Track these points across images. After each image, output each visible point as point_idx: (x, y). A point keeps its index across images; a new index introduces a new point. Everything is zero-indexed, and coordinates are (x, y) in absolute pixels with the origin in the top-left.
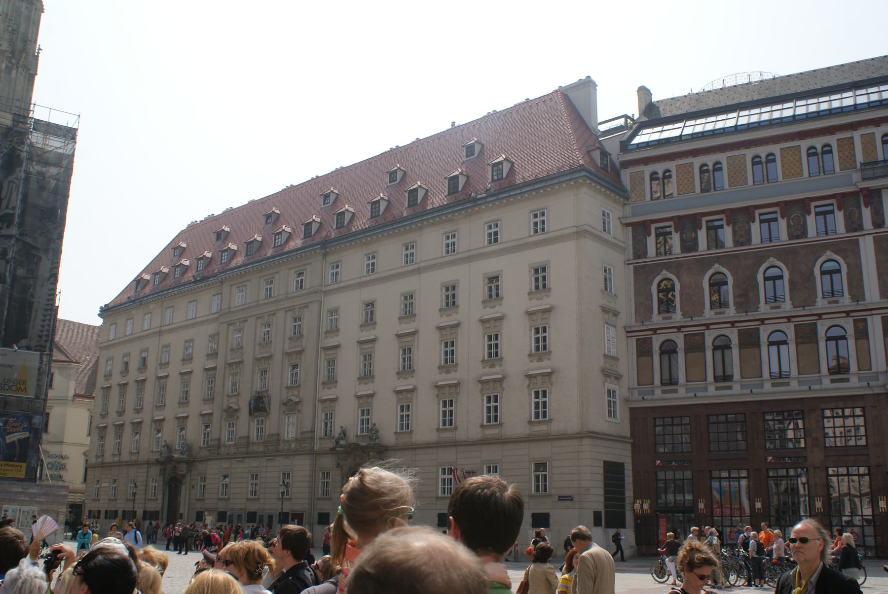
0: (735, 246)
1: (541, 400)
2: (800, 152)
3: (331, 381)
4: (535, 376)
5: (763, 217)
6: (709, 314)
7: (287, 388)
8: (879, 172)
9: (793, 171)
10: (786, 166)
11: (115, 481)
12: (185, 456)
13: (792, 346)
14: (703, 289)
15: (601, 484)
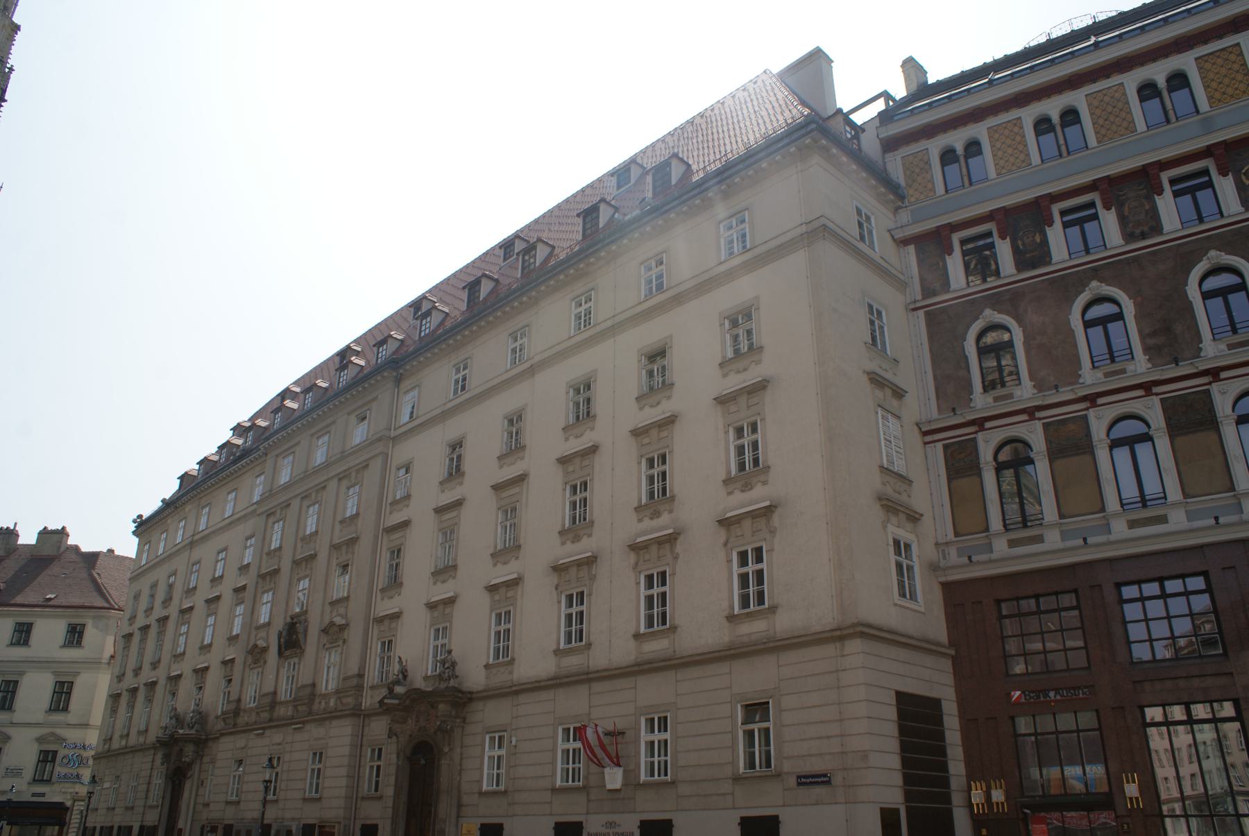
1: (751, 568)
3: (395, 583)
4: (739, 519)
6: (1090, 378)
9: (1230, 91)
11: (118, 777)
12: (193, 732)
13: (1163, 443)
14: (1071, 333)
15: (894, 745)
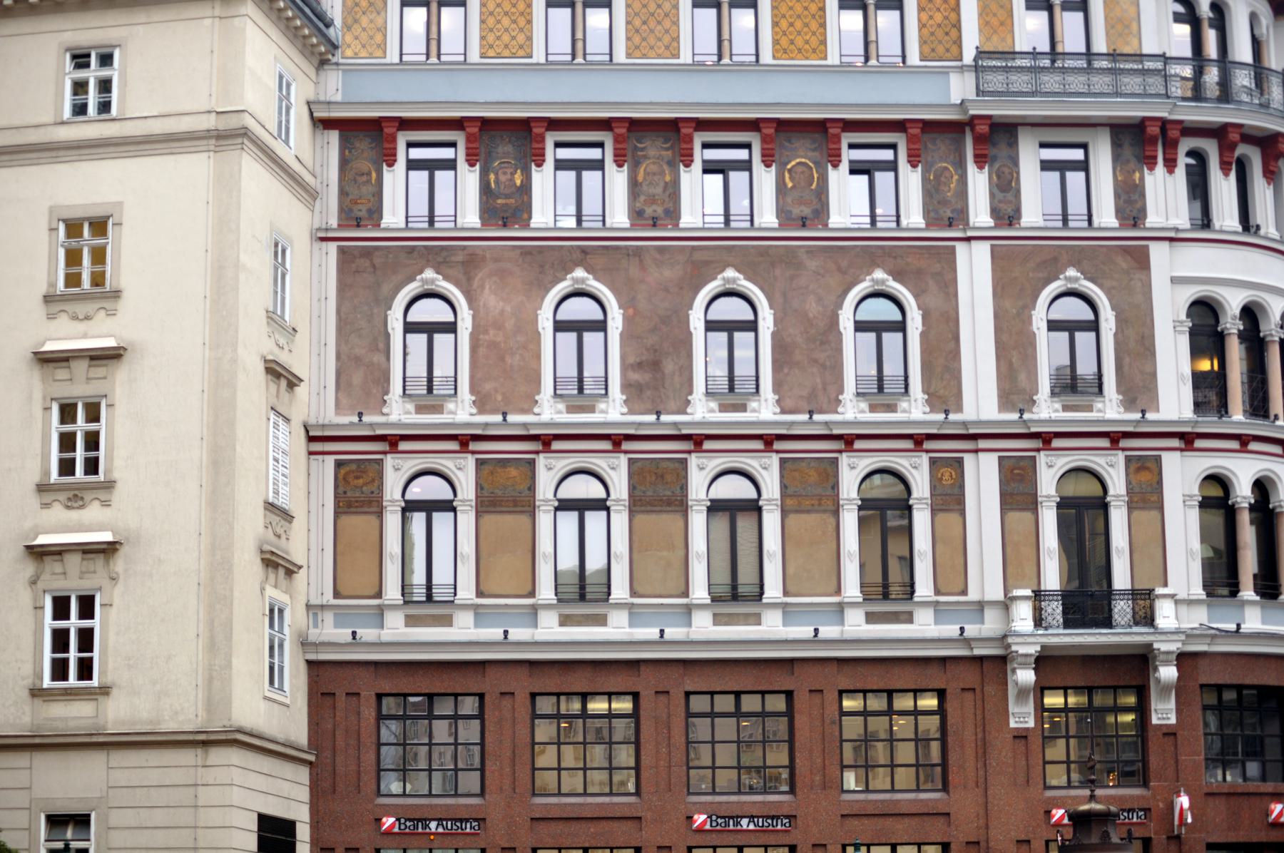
1: (74, 622)
4: (58, 552)
5: (416, 153)
9: (799, 42)
10: (784, 24)
14: (537, 336)
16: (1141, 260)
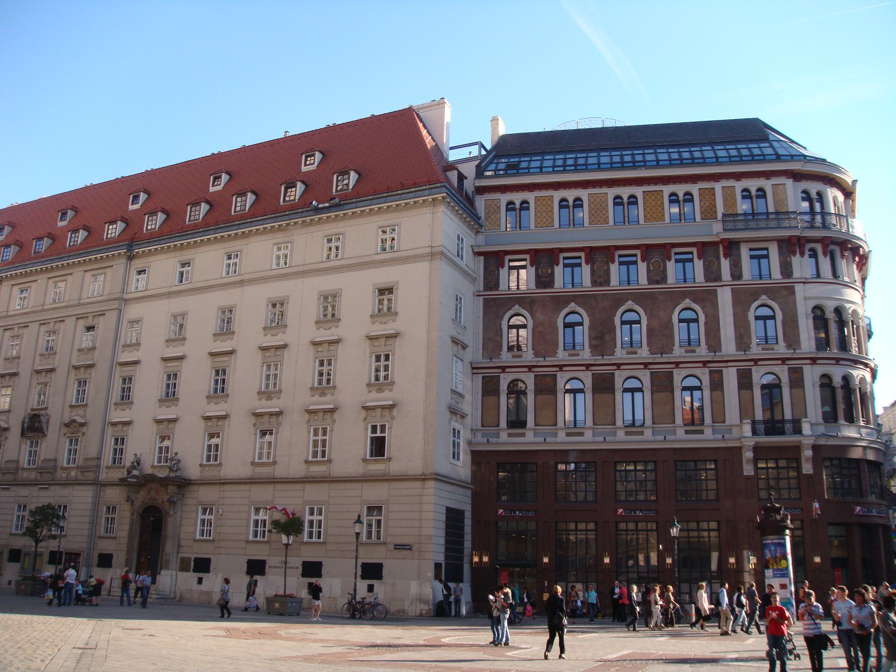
0: (593, 286)
1: (320, 437)
2: (662, 197)
4: (373, 408)
6: (562, 355)
7: (71, 406)
8: (740, 225)
9: (654, 216)
10: (648, 209)
13: (589, 395)
15: (442, 533)
16: (791, 291)
